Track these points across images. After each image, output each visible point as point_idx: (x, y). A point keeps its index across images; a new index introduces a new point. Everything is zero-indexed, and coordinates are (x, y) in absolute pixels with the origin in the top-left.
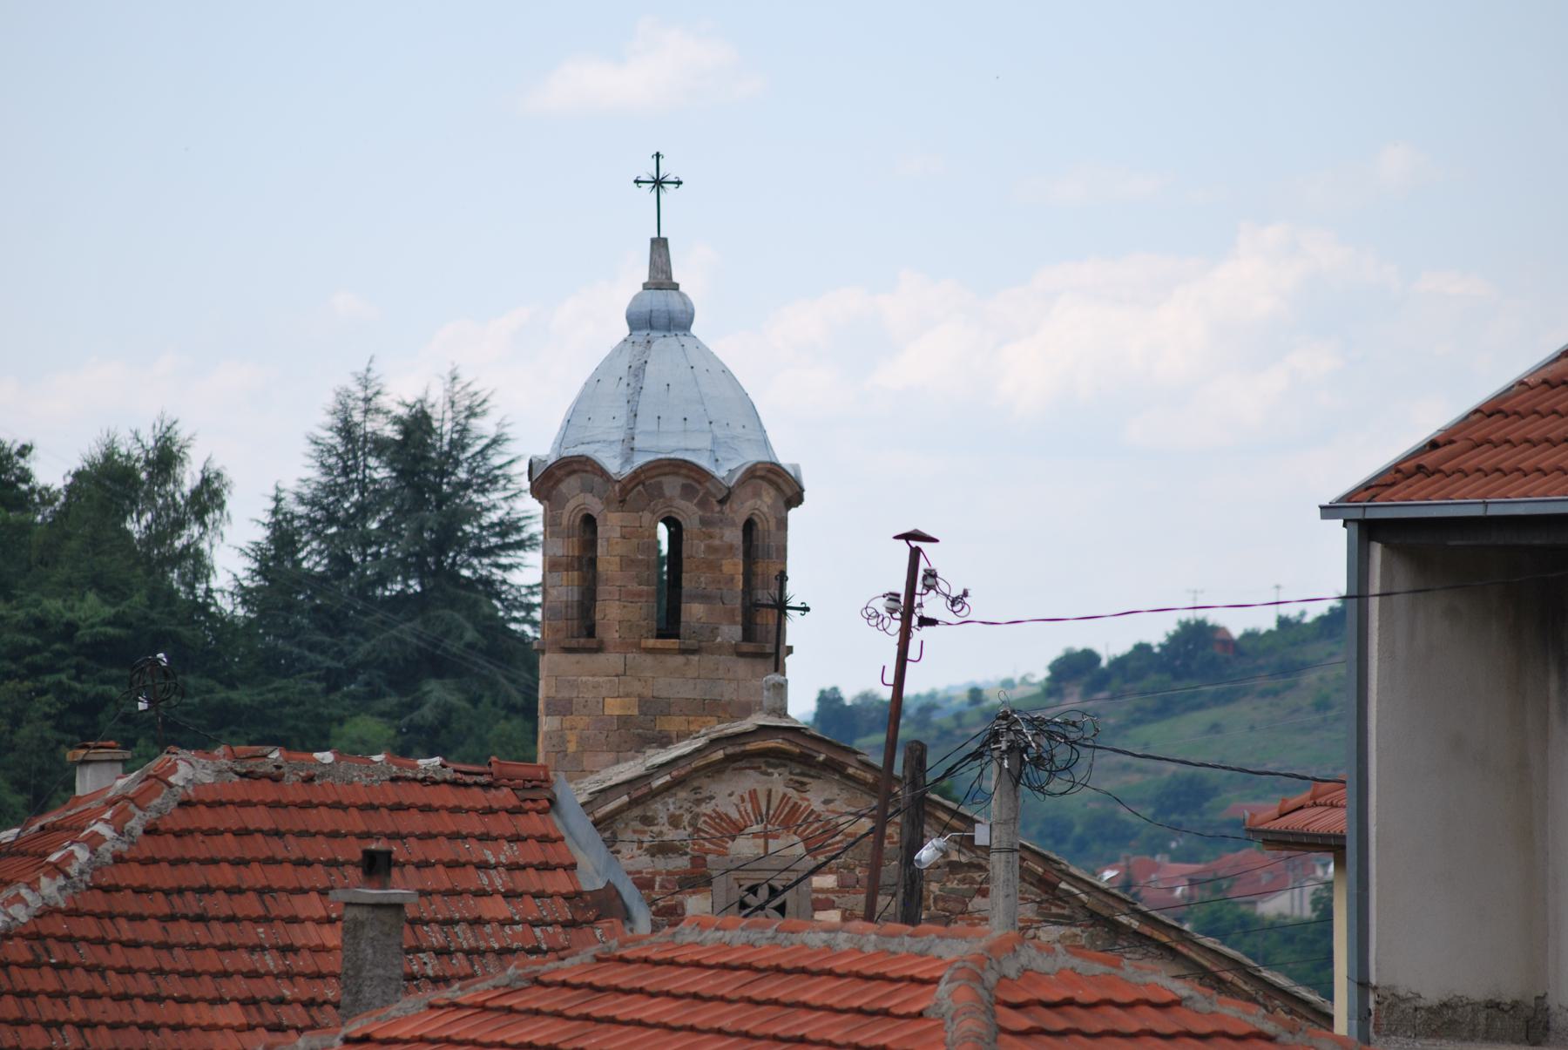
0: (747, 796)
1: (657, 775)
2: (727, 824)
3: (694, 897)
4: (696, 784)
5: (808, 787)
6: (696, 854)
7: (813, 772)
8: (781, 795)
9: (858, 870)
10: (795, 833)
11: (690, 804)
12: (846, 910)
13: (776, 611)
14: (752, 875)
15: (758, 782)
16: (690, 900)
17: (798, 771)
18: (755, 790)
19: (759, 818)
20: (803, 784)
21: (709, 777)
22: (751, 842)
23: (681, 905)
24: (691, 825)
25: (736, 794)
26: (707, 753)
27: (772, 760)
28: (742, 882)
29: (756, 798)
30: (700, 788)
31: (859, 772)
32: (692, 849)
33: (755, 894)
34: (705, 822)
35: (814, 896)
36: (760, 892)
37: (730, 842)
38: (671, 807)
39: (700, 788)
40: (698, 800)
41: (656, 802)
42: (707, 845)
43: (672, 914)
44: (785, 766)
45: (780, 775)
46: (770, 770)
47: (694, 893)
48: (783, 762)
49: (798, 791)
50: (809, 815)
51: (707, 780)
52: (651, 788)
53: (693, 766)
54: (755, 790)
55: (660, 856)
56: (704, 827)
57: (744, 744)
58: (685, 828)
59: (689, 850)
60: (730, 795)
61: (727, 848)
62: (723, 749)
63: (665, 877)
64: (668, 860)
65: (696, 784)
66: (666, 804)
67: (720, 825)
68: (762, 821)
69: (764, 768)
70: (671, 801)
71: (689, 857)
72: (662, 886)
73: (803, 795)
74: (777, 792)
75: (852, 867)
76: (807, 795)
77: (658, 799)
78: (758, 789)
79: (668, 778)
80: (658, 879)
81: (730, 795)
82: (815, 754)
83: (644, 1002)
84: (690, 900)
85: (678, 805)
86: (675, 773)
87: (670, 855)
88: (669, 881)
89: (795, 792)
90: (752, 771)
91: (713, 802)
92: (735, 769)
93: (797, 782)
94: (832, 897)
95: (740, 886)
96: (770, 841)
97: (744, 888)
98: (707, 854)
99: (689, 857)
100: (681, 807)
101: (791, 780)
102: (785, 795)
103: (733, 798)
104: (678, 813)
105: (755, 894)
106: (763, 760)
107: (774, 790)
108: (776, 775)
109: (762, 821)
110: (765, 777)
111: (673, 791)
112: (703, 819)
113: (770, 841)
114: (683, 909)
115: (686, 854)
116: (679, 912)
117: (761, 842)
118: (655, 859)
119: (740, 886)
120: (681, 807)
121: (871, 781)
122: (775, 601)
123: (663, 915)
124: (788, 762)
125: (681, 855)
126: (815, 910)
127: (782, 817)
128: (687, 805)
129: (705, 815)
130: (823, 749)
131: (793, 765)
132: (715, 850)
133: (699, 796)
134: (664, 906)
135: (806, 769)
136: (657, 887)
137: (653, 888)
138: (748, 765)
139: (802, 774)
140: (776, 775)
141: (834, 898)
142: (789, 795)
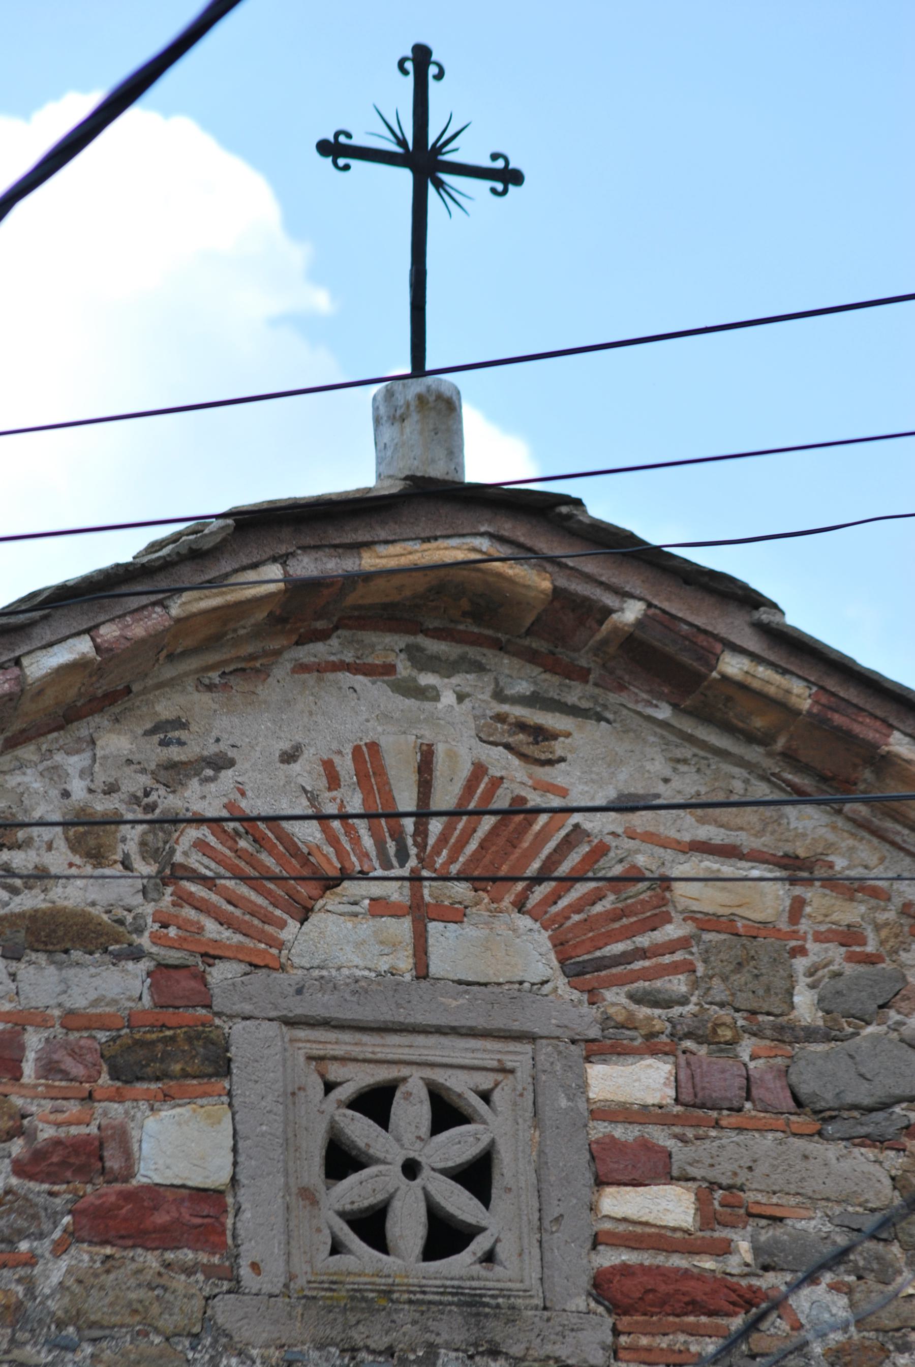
0: (346, 766)
1: (45, 633)
2: (278, 858)
3: (167, 1113)
4: (165, 709)
5: (559, 747)
6: (174, 956)
7: (575, 695)
8: (465, 770)
9: (746, 1048)
10: (520, 906)
11: (146, 780)
12: (714, 1185)
13: (404, 177)
14: (371, 1044)
15: (385, 717)
16: (151, 1124)
17: (523, 687)
18: (373, 747)
19: (391, 847)
20: (540, 734)
21: (210, 688)
22: (367, 927)
23: (122, 1137)
24: (148, 851)
25: (308, 753)
26: (226, 566)
27: (434, 646)
28: (335, 1072)
29: (380, 772)
30: (179, 724)
31: (762, 671)
32: (155, 939)
33: (382, 1118)
34: (200, 845)
35: (599, 1130)
36: (399, 1109)
37: (293, 925)
38: (78, 788)
39: (179, 724)
40: (172, 766)
41: (21, 766)
42: (212, 928)
43: (84, 1172)
44: (479, 668)
45: (461, 698)
46: (427, 679)
47: (167, 1097)
48: (473, 652)
49: (522, 756)
50: (567, 844)
51: (206, 698)
52: (20, 680)
53: (175, 610)
54: (373, 747)
55: (42, 958)
56: (197, 862)
57: (357, 547)
58: (126, 864)
59: (144, 941)
60: (289, 757)
61: (280, 945)
62: (282, 559)
63: (59, 1030)
64: (70, 972)
65: (165, 709)
66: (55, 773)
67: (251, 861)
68: (403, 856)
69: (404, 669)
70: (74, 763)
71: (145, 965)
72: (49, 1068)
73: (544, 773)
74: (452, 756)
75: (726, 1034)
76: (557, 775)
77: (27, 752)
78: (385, 742)
79: (83, 646)
80: (34, 1040)
81: (289, 757)
82: (609, 600)
83: (332, 1035)
84: (151, 1124)
85: (101, 777)
86: (109, 632)
87: (76, 955)
88: (75, 1053)
89: (515, 762)
90: (360, 680)
91: (227, 776)
92: (302, 668)
93: (522, 726)
94: (661, 1137)
95: (329, 1087)
96: (434, 928)
97: (345, 1092)
98: (210, 958)
99: (145, 965)
100: (111, 789)
101: (500, 718)
102: (479, 770)
103: (296, 767)
104: (102, 806)
105: (382, 1118)
106: (400, 641)
107: (440, 749)
108: (448, 698)
109: (403, 856)
110: (410, 703)
111: (83, 729)
112: (193, 833)
113: (434, 928)
114: (127, 1154)
115: (136, 955)
116: (114, 1163)
117: (403, 928)
118: (23, 969)
119: (329, 1087)
120: (111, 789)
121: (806, 705)
122: (402, 142)
123: (51, 1177)
124: (490, 657)
125: (118, 957)
126: (600, 1182)
127: (473, 846)
128: (135, 782)
129: (199, 820)
130: (632, 581)
131: (506, 664)
132: (240, 947)
133: (175, 753)
134: (57, 1143)
135: (550, 684)
136: (29, 1069)
137: (17, 1075)
138: (349, 657)
139: (534, 700)
140: (448, 698)
141: (671, 1144)
142: (495, 772)
